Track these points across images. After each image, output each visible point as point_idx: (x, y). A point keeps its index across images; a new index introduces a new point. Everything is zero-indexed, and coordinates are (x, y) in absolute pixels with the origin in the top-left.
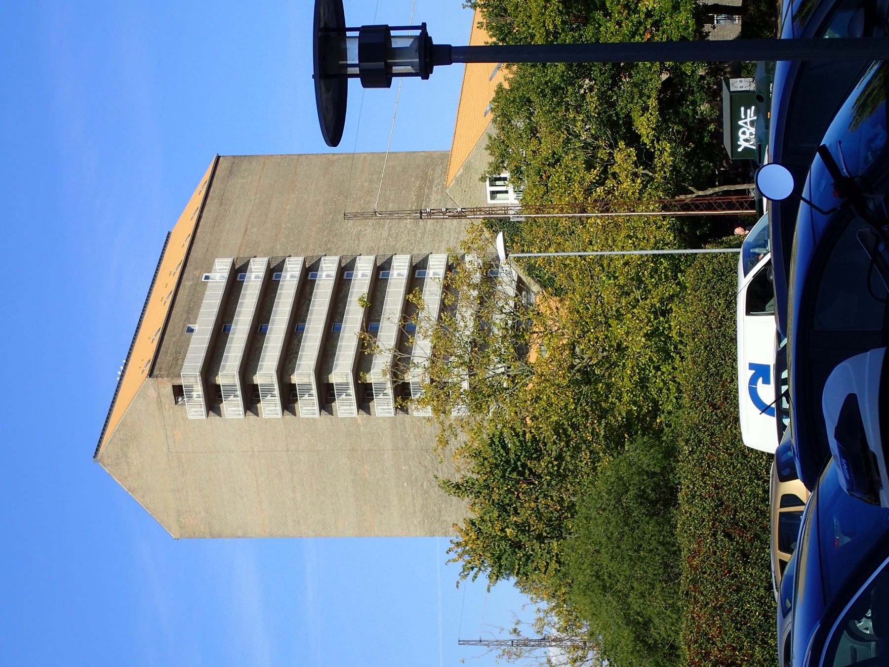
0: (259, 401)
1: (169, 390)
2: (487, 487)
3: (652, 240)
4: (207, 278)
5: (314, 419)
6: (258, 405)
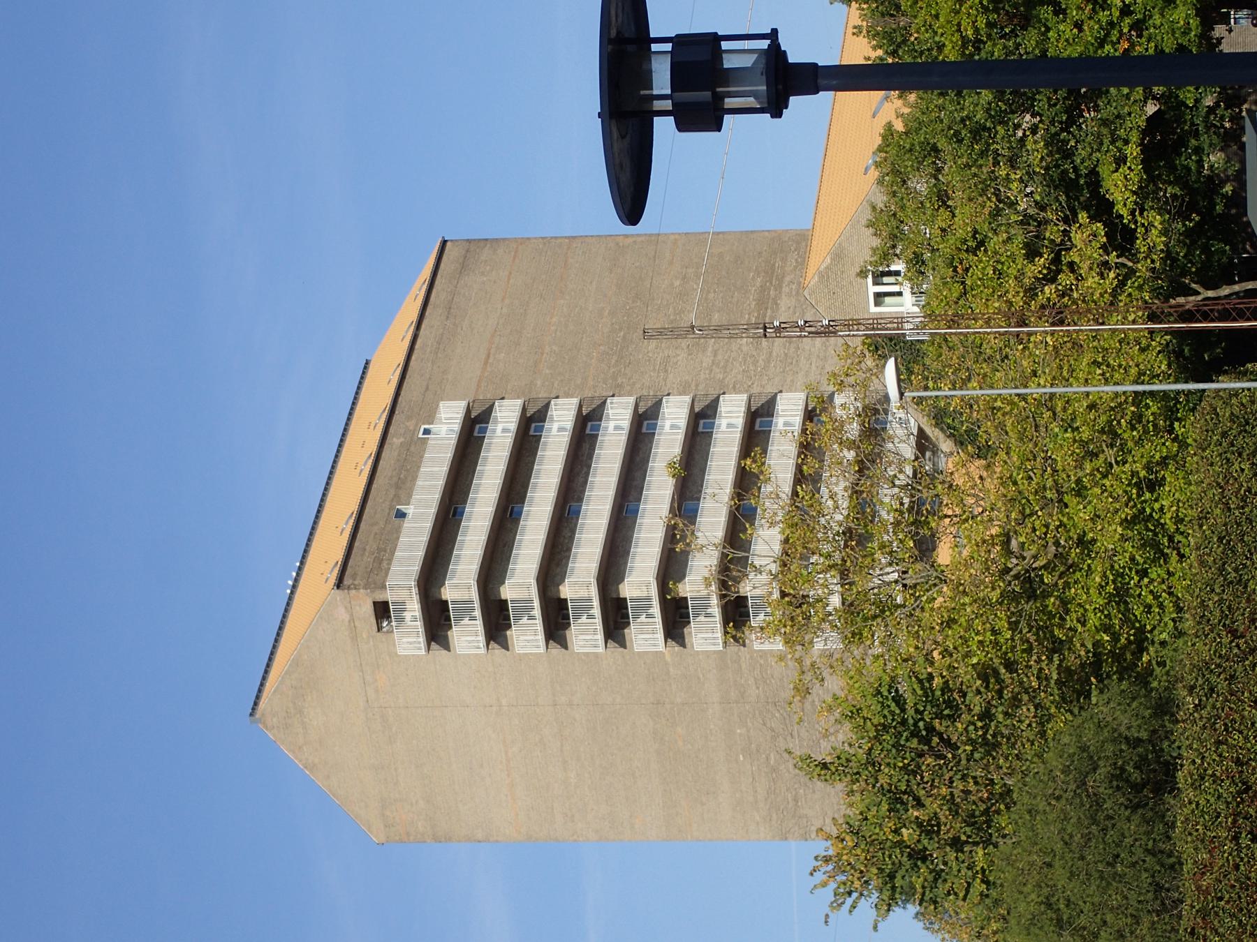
0: (509, 626)
1: (367, 610)
4: (427, 432)
5: (596, 655)
6: (508, 633)
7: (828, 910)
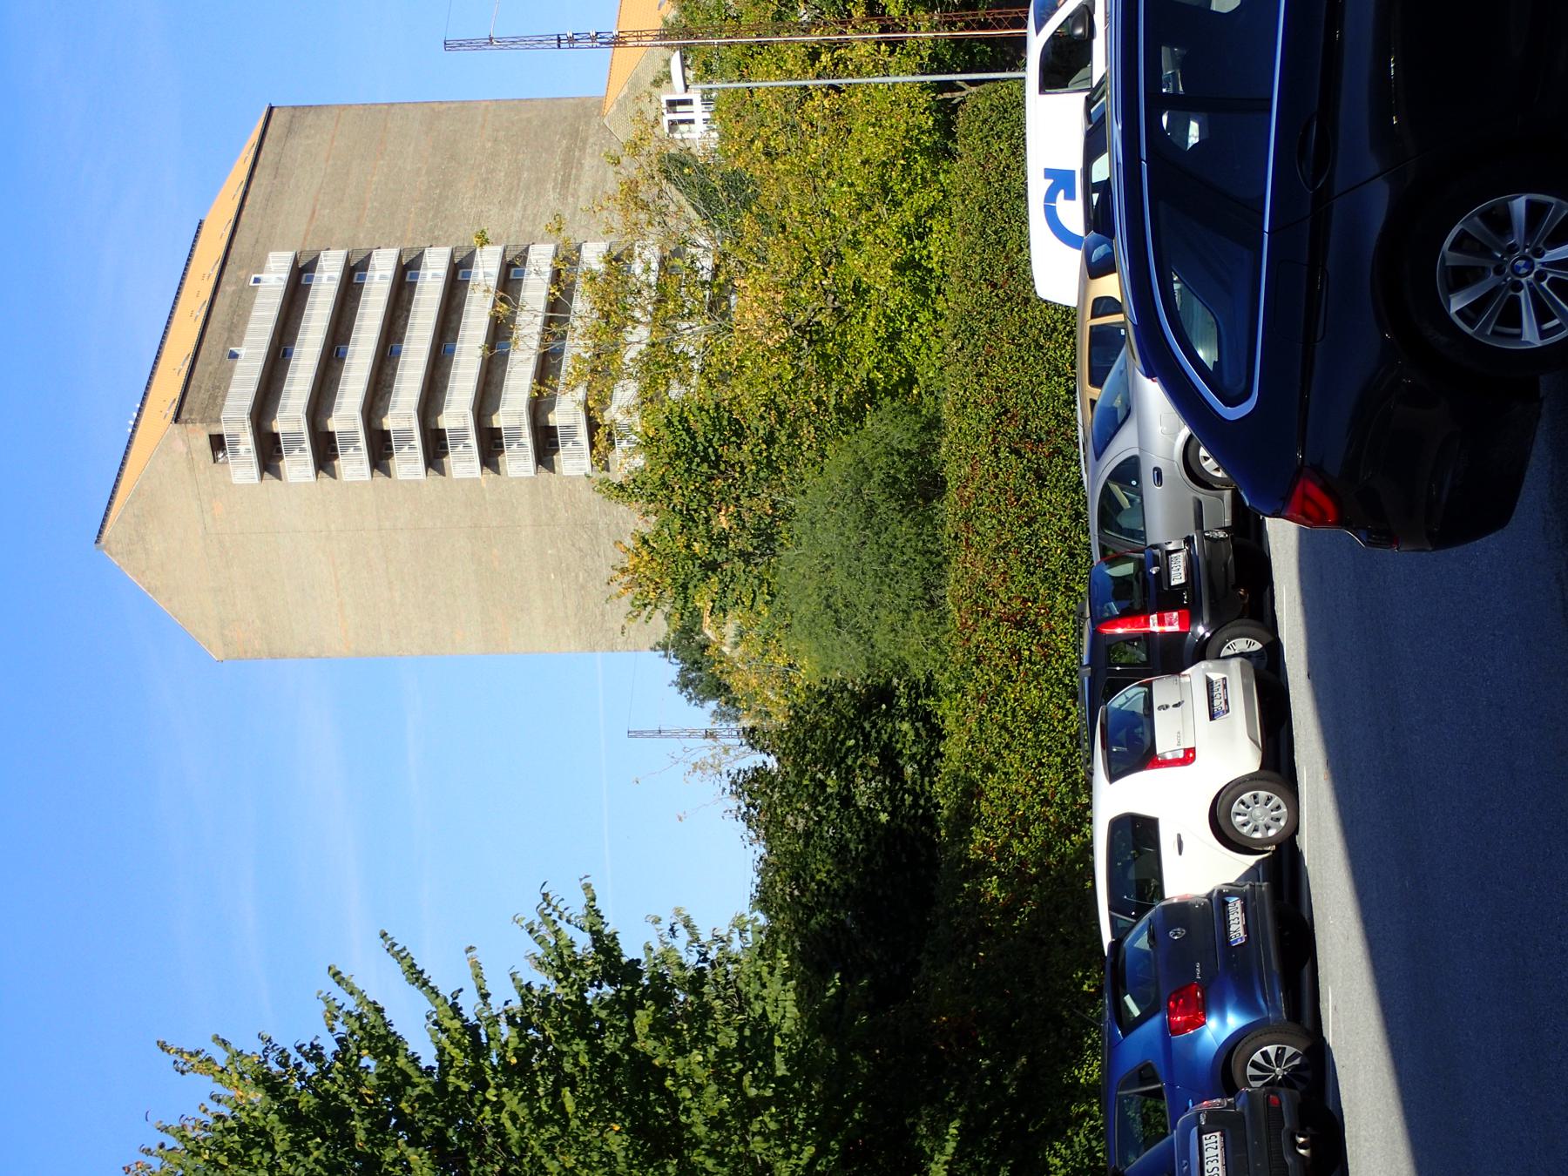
0: (336, 457)
1: (204, 442)
2: (664, 485)
3: (903, 127)
4: (257, 280)
5: (418, 482)
7: (623, 621)
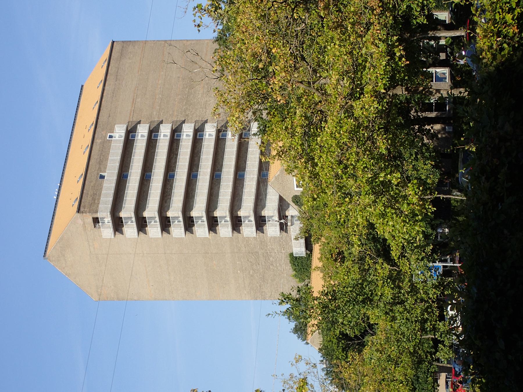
1: (91, 220)
4: (111, 137)
